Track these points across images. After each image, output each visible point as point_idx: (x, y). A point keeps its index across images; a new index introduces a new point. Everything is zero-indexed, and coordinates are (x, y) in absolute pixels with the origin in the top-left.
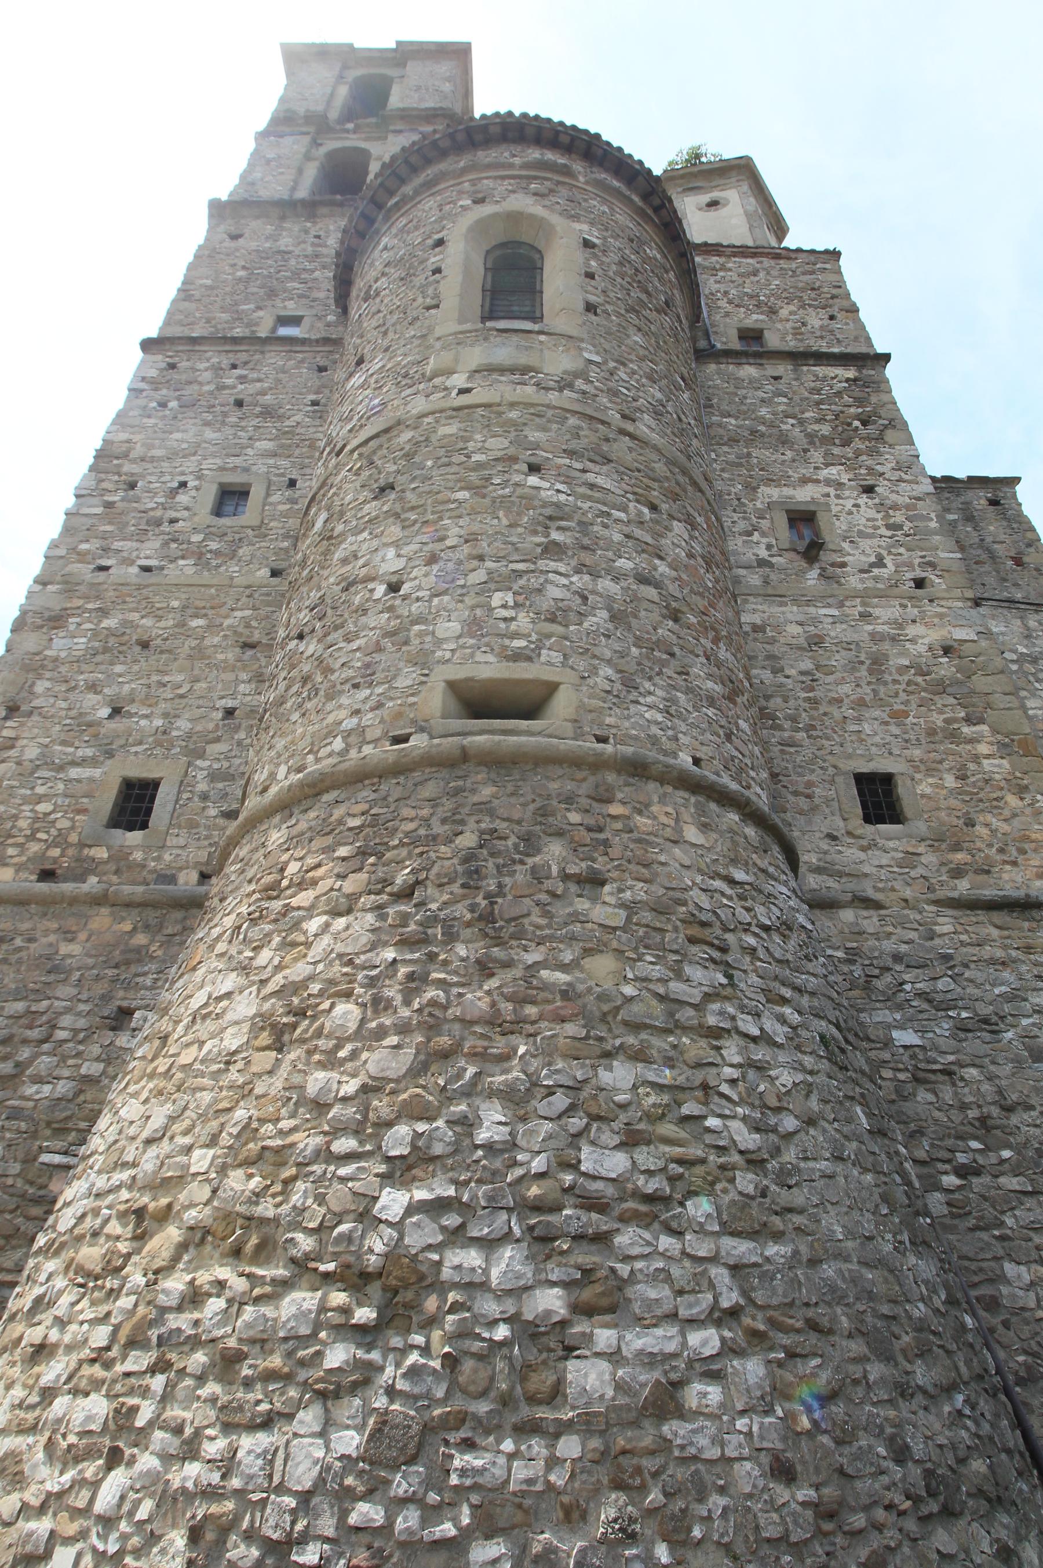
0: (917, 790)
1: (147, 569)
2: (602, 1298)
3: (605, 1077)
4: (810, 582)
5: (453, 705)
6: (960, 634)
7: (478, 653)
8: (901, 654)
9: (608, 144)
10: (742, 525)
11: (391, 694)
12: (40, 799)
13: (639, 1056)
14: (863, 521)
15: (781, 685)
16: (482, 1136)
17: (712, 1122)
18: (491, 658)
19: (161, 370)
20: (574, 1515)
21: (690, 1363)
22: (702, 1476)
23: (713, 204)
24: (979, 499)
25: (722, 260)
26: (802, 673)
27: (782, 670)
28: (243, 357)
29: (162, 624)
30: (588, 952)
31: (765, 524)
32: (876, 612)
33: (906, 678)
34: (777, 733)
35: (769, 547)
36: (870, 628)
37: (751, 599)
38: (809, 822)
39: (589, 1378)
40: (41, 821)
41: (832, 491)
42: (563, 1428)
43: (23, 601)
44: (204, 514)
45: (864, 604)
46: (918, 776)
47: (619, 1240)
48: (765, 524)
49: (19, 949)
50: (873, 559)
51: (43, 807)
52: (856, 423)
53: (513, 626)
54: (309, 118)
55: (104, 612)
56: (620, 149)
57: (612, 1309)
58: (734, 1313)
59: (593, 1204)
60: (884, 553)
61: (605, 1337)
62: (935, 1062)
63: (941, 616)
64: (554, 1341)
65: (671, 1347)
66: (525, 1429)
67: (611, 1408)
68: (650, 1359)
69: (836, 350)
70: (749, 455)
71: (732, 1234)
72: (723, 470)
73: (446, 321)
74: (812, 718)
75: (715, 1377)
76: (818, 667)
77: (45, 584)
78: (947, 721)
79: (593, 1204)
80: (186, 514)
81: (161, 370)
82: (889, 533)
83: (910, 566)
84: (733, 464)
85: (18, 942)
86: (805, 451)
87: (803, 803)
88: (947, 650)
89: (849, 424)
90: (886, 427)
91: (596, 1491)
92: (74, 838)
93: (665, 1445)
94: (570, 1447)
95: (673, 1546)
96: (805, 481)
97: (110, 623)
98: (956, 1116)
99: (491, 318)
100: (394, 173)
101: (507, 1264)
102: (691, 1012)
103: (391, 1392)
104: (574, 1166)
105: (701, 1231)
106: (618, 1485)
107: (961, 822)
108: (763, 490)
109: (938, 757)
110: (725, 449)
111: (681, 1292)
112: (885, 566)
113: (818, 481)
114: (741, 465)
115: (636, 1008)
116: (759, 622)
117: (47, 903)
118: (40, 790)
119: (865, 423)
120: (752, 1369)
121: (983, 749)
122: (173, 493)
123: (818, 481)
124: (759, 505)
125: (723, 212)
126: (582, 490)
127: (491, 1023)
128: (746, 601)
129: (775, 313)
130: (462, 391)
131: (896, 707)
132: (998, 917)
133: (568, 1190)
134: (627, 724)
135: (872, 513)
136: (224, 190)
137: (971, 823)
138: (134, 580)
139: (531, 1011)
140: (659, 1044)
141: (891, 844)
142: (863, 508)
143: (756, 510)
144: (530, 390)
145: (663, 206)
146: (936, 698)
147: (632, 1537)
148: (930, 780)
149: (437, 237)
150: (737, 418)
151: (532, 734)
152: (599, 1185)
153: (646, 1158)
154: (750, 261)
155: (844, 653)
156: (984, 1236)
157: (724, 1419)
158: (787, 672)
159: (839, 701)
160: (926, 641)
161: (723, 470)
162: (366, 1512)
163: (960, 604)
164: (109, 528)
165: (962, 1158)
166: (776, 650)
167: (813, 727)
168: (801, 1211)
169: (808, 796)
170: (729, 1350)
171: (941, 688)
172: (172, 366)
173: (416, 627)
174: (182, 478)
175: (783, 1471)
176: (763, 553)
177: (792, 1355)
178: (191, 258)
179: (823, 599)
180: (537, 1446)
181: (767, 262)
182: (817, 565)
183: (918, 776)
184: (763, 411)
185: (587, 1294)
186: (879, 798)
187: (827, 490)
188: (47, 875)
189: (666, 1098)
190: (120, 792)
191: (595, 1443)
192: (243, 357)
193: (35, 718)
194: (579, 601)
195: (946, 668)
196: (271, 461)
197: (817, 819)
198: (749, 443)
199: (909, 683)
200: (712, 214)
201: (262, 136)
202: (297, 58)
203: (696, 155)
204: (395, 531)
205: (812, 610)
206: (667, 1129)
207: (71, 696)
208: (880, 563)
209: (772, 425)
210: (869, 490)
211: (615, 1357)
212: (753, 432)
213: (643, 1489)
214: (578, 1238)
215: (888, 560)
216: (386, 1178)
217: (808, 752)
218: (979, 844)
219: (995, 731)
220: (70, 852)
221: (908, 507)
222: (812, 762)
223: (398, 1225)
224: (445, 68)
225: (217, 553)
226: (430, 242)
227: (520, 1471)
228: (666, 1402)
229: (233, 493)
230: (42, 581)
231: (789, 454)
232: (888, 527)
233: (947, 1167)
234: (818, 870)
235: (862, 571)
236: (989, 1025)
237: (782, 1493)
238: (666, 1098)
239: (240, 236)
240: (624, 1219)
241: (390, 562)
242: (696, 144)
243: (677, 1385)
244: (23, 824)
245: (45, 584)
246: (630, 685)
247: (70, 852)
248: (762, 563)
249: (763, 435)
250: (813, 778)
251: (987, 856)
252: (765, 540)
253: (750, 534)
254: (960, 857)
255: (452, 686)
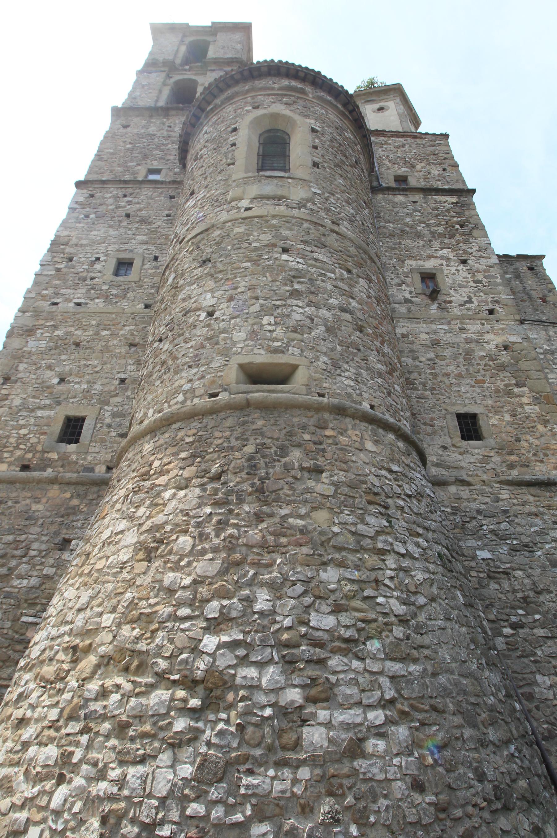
0: (490, 422)
1: (78, 304)
2: (321, 694)
3: (323, 576)
4: (433, 311)
5: (242, 377)
6: (513, 339)
7: (255, 349)
8: (481, 350)
9: (325, 77)
10: (396, 281)
11: (209, 371)
12: (21, 427)
13: (341, 564)
14: (461, 278)
15: (417, 366)
16: (258, 607)
17: (380, 600)
18: (262, 352)
19: (86, 198)
20: (307, 810)
21: (369, 729)
22: (375, 789)
23: (381, 109)
24: (523, 267)
25: (385, 139)
26: (428, 360)
27: (418, 358)
28: (130, 191)
29: (87, 333)
30: (314, 509)
31: (408, 280)
32: (468, 327)
33: (484, 362)
34: (415, 392)
35: (411, 292)
36: (465, 335)
37: (401, 320)
38: (432, 439)
39: (314, 736)
40: (22, 439)
41: (444, 262)
42: (301, 763)
43: (12, 321)
44: (109, 275)
45: (461, 323)
46: (490, 415)
47: (330, 663)
48: (408, 280)
49: (10, 507)
50: (466, 299)
51: (23, 432)
52: (457, 226)
53: (274, 335)
54: (165, 63)
55: (55, 327)
56: (331, 80)
57: (327, 700)
58: (392, 701)
59: (317, 643)
60: (472, 295)
61: (323, 715)
62: (500, 568)
63: (503, 329)
64: (296, 717)
65: (358, 720)
66: (280, 764)
67: (327, 753)
68: (347, 726)
69: (446, 187)
70: (400, 243)
71: (391, 660)
72: (386, 251)
73: (238, 172)
74: (433, 384)
75: (382, 736)
76: (437, 357)
77: (24, 312)
78: (506, 385)
79: (317, 643)
80: (99, 274)
81: (86, 198)
82: (475, 285)
83: (486, 302)
84: (391, 248)
85: (10, 503)
86: (430, 241)
87: (429, 429)
88: (506, 348)
89: (454, 227)
90: (473, 228)
91: (318, 797)
92: (39, 448)
93: (355, 772)
94: (304, 773)
95: (360, 826)
96: (430, 257)
97: (59, 333)
98: (511, 597)
99: (262, 170)
100: (210, 93)
101: (271, 675)
102: (369, 541)
103: (209, 744)
104: (306, 623)
105: (374, 658)
106: (330, 794)
107: (513, 439)
108: (408, 262)
109: (501, 405)
110: (387, 240)
111: (363, 691)
112: (472, 302)
113: (437, 257)
114: (396, 248)
115: (340, 539)
116: (405, 332)
117: (25, 482)
118: (21, 422)
119: (462, 226)
120: (402, 732)
121: (525, 400)
122: (93, 263)
123: (437, 257)
124: (405, 270)
125: (386, 113)
126: (311, 262)
127: (262, 547)
128: (398, 321)
129: (414, 167)
130: (247, 209)
131: (478, 378)
132: (533, 490)
133: (303, 636)
134: (335, 387)
135: (466, 274)
136: (119, 101)
137: (518, 440)
138: (72, 310)
139: (284, 540)
140: (352, 558)
141: (476, 451)
142: (461, 272)
143: (404, 272)
144: (283, 208)
145: (354, 110)
146: (500, 373)
147: (338, 822)
148: (497, 417)
149: (233, 126)
150: (393, 223)
151: (284, 392)
152: (320, 633)
153: (345, 619)
154: (400, 139)
155: (450, 349)
156: (526, 660)
157: (387, 759)
158: (421, 359)
159: (448, 375)
160: (495, 342)
161: (386, 251)
162: (196, 808)
163: (513, 323)
164: (58, 282)
165: (513, 619)
166: (414, 347)
167: (434, 389)
168: (428, 647)
169: (432, 426)
170: (389, 721)
171: (502, 367)
172: (92, 196)
173: (222, 335)
174: (97, 256)
175: (418, 786)
176: (408, 296)
177: (423, 724)
178: (102, 138)
179: (439, 320)
180: (287, 773)
181: (410, 140)
182: (436, 302)
183: (490, 415)
184: (408, 220)
185: (313, 692)
186: (469, 427)
187: (442, 262)
188: (25, 468)
189: (355, 587)
190: (64, 423)
191: (318, 771)
192: (130, 191)
193: (19, 384)
194: (309, 321)
195: (505, 357)
196: (145, 247)
197: (436, 438)
198: (400, 237)
199: (485, 365)
200: (380, 114)
201: (140, 73)
202: (159, 31)
203: (372, 83)
204: (211, 284)
205: (433, 326)
206: (356, 603)
207: (38, 372)
208: (470, 301)
209: (412, 227)
210: (464, 262)
211: (328, 725)
212: (402, 231)
213: (343, 796)
214: (309, 662)
215: (474, 299)
216: (206, 630)
217: (431, 402)
218: (523, 451)
219: (531, 391)
220: (38, 455)
221: (485, 271)
222: (434, 407)
223: (213, 655)
224: (237, 36)
225: (116, 296)
226: (230, 129)
227: (278, 786)
228: (356, 749)
229: (125, 263)
230: (22, 311)
231: (422, 243)
232: (474, 282)
233: (506, 624)
234: (437, 465)
235: (460, 305)
236: (528, 548)
237: (418, 798)
238: (355, 587)
239: (128, 126)
240: (333, 651)
241: (208, 300)
242: (372, 77)
243: (362, 740)
244: (12, 440)
245: (24, 312)
246: (336, 366)
247: (38, 455)
248: (407, 301)
249: (407, 233)
250: (434, 416)
251: (527, 458)
252: (408, 289)
253: (401, 285)
254: (513, 458)
255: (242, 367)
